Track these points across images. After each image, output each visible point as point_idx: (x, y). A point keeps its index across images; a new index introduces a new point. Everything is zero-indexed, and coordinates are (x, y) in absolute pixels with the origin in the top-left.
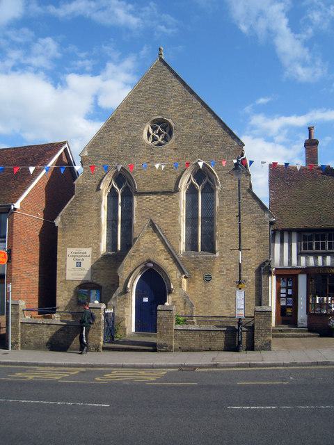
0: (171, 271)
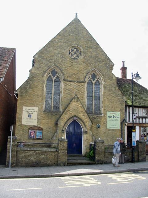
0: (86, 122)
